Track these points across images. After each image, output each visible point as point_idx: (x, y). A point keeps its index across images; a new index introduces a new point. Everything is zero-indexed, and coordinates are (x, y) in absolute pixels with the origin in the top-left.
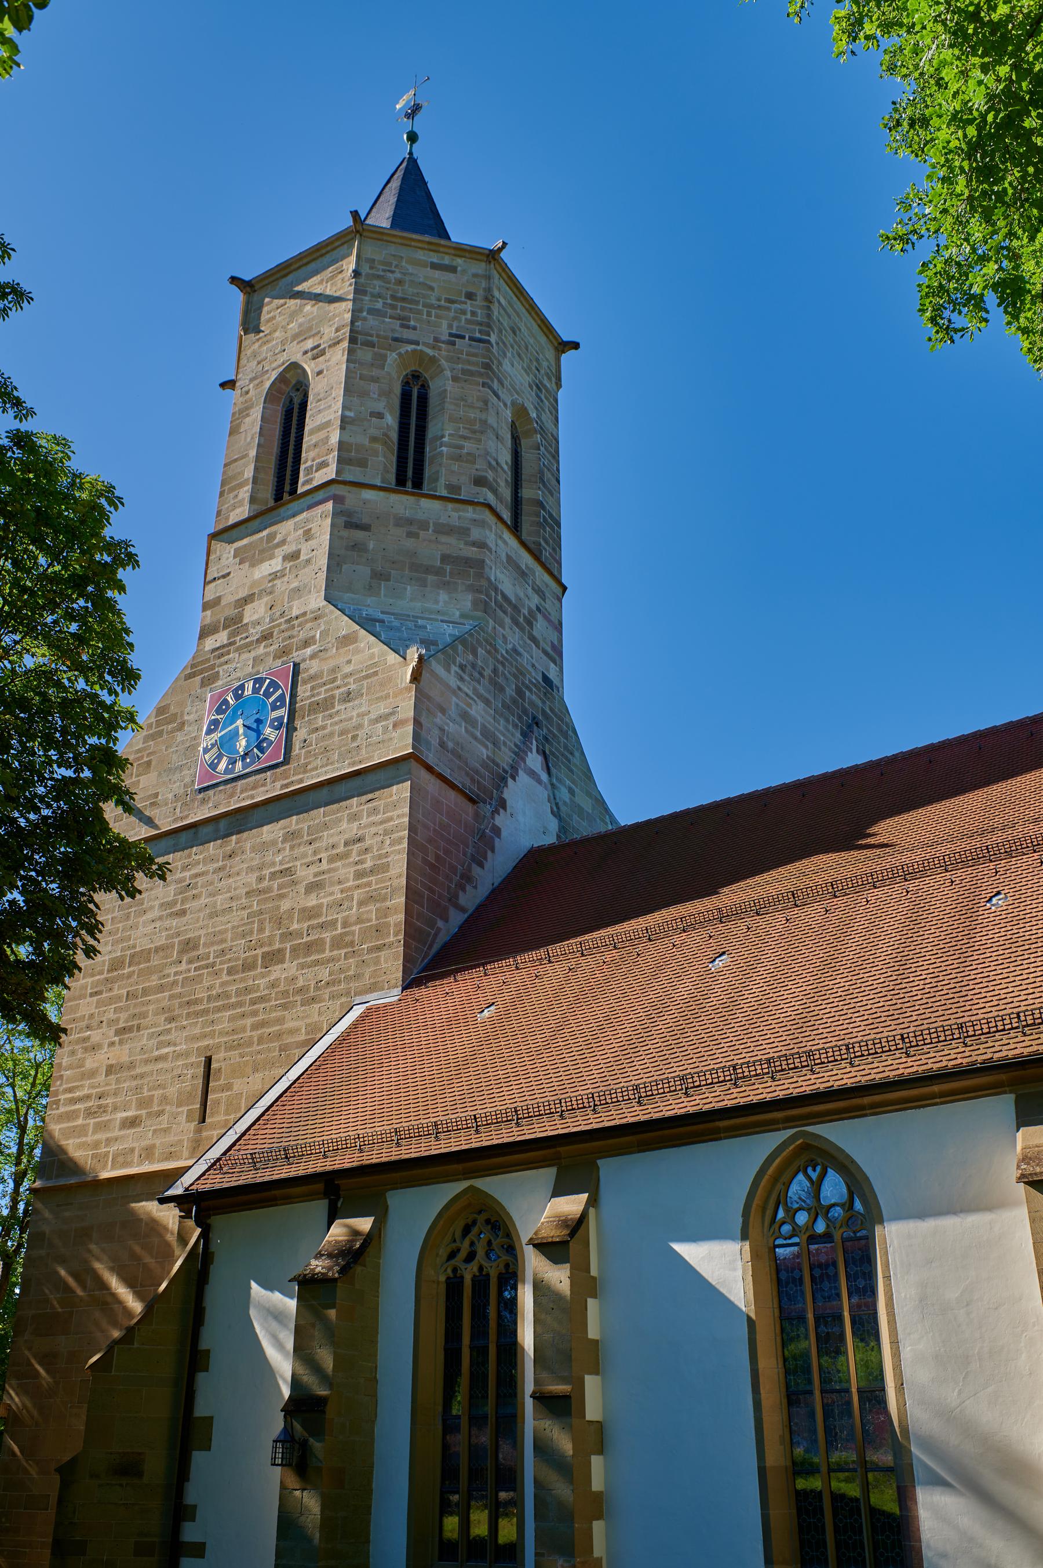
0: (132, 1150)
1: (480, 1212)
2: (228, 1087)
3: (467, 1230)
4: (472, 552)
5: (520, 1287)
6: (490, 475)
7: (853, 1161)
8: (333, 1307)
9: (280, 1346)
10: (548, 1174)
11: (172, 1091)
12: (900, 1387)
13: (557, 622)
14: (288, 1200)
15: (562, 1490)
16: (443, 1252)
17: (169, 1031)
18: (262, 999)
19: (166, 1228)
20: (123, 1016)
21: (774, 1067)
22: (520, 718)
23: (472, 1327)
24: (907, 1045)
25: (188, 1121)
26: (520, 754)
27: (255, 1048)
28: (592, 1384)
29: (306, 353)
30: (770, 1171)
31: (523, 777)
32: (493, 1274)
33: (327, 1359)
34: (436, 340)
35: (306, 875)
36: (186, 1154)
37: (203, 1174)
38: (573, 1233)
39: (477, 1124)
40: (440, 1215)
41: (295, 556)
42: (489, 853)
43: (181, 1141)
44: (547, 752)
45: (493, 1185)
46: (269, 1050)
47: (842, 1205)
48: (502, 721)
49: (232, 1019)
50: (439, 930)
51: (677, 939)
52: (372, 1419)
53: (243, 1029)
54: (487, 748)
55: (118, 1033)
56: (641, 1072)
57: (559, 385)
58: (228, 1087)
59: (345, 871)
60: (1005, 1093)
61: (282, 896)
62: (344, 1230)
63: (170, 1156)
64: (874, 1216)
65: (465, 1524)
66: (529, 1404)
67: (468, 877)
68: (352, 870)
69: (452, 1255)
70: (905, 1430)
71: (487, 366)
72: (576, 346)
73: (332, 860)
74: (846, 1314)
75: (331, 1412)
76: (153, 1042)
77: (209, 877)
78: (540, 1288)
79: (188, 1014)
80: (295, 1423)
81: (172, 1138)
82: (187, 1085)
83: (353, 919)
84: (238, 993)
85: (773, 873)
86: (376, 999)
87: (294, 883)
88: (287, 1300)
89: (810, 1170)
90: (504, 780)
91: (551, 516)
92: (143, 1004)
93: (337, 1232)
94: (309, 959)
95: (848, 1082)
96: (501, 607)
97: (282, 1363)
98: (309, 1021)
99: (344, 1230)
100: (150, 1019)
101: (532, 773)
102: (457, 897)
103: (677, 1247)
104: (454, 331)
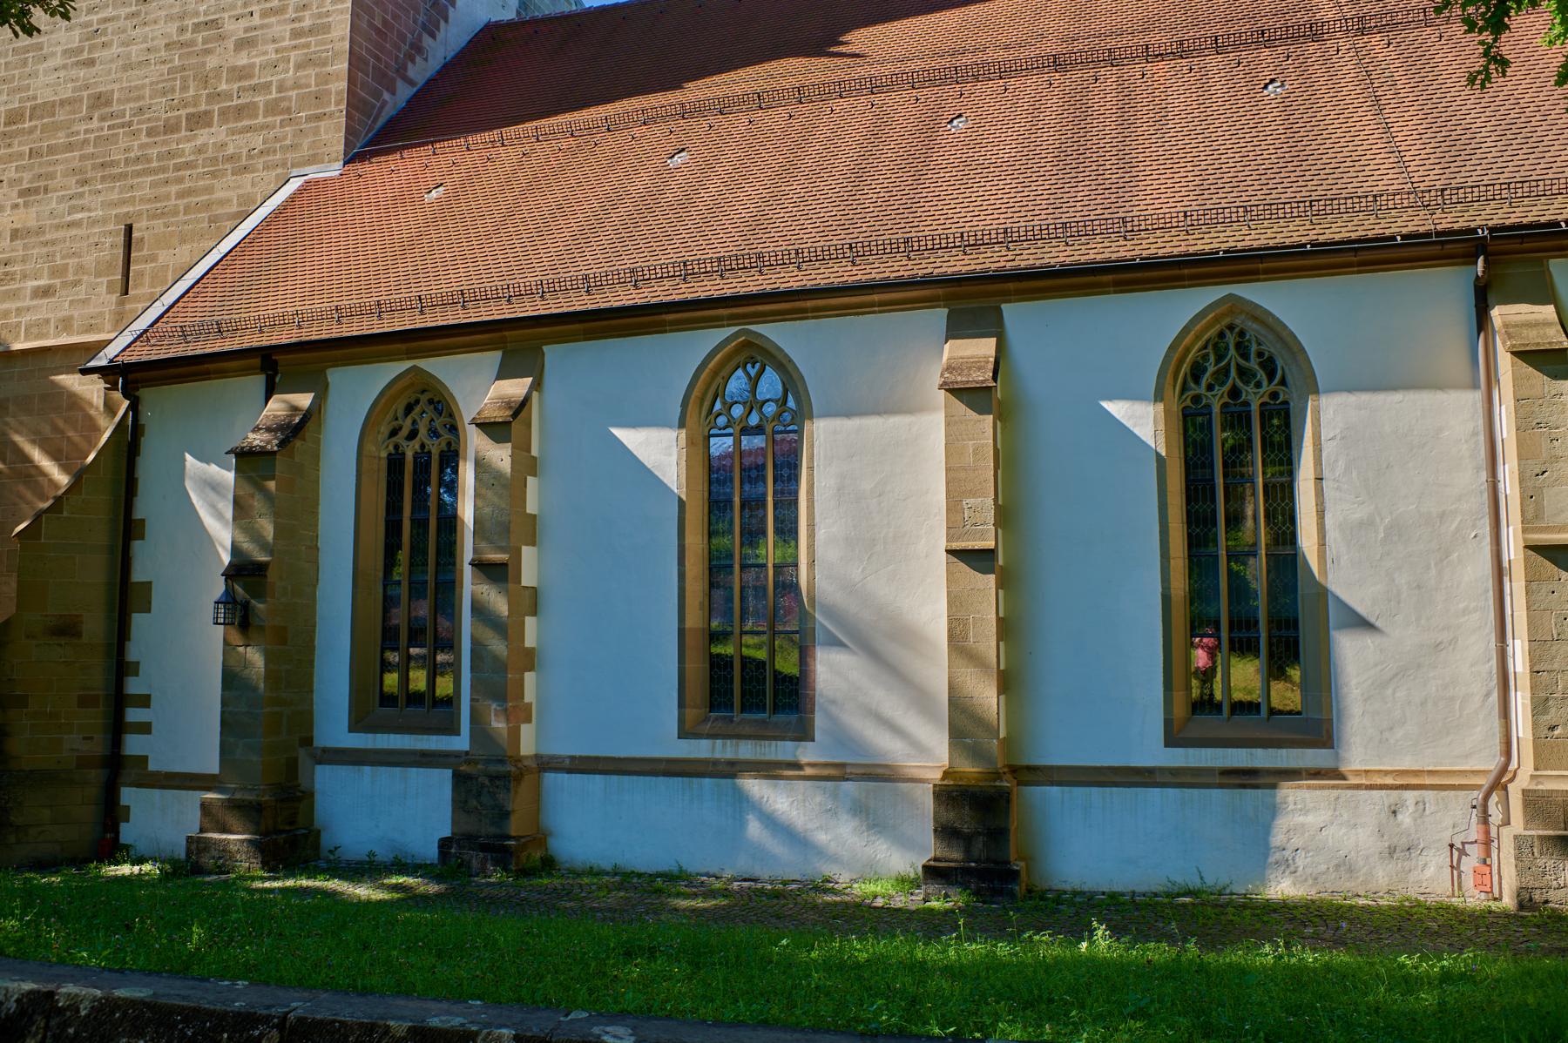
0: (47, 321)
1: (423, 392)
2: (153, 258)
3: (409, 409)
5: (461, 464)
7: (790, 361)
8: (273, 478)
9: (219, 516)
10: (494, 358)
11: (89, 260)
12: (812, 563)
14: (223, 374)
15: (498, 646)
16: (385, 430)
17: (81, 195)
18: (188, 165)
19: (91, 404)
20: (27, 176)
21: (724, 267)
23: (413, 501)
24: (854, 252)
25: (109, 292)
27: (181, 217)
28: (528, 553)
30: (711, 365)
32: (435, 452)
33: (268, 529)
35: (235, 29)
36: (108, 326)
37: (129, 346)
38: (515, 415)
39: (422, 305)
40: (382, 393)
42: (442, 23)
43: (101, 314)
45: (435, 366)
46: (198, 221)
47: (776, 401)
49: (153, 185)
50: (385, 103)
51: (636, 132)
52: (314, 583)
53: (168, 197)
55: (21, 194)
56: (591, 263)
58: (153, 258)
59: (280, 28)
61: (208, 52)
62: (283, 406)
63: (90, 328)
64: (804, 412)
65: (405, 680)
66: (467, 571)
67: (417, 48)
68: (289, 27)
69: (394, 433)
70: (812, 600)
73: (264, 14)
74: (770, 499)
75: (272, 575)
76: (64, 206)
77: (121, 23)
78: (480, 465)
79: (103, 177)
80: (237, 587)
81: (91, 310)
82: (105, 254)
83: (290, 83)
84: (160, 157)
85: (741, 72)
86: (315, 173)
87: (221, 37)
88: (224, 472)
89: (749, 367)
92: (49, 163)
93: (276, 407)
94: (240, 124)
95: (795, 285)
97: (222, 534)
98: (241, 192)
99: (283, 406)
100: (59, 181)
102: (405, 69)
103: (618, 432)
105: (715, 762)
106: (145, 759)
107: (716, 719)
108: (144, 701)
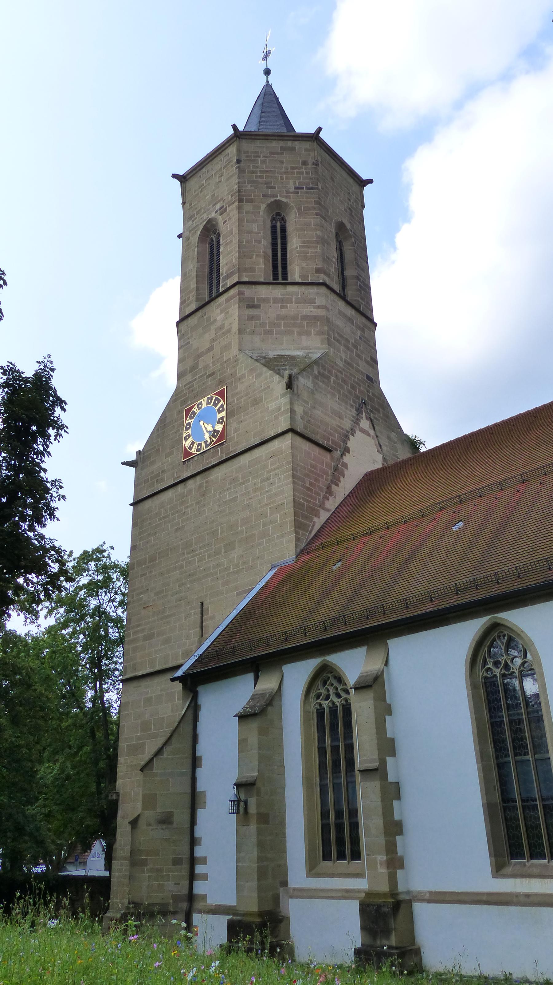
22: (354, 401)
26: (356, 421)
29: (217, 212)
31: (358, 434)
34: (287, 192)
41: (221, 327)
44: (372, 418)
48: (343, 404)
54: (335, 420)
60: (239, 888)
90: (347, 437)
96: (338, 341)
101: (363, 431)
102: (324, 503)
104: (297, 186)
105: (517, 895)
106: (204, 897)
107: (515, 864)
108: (204, 861)
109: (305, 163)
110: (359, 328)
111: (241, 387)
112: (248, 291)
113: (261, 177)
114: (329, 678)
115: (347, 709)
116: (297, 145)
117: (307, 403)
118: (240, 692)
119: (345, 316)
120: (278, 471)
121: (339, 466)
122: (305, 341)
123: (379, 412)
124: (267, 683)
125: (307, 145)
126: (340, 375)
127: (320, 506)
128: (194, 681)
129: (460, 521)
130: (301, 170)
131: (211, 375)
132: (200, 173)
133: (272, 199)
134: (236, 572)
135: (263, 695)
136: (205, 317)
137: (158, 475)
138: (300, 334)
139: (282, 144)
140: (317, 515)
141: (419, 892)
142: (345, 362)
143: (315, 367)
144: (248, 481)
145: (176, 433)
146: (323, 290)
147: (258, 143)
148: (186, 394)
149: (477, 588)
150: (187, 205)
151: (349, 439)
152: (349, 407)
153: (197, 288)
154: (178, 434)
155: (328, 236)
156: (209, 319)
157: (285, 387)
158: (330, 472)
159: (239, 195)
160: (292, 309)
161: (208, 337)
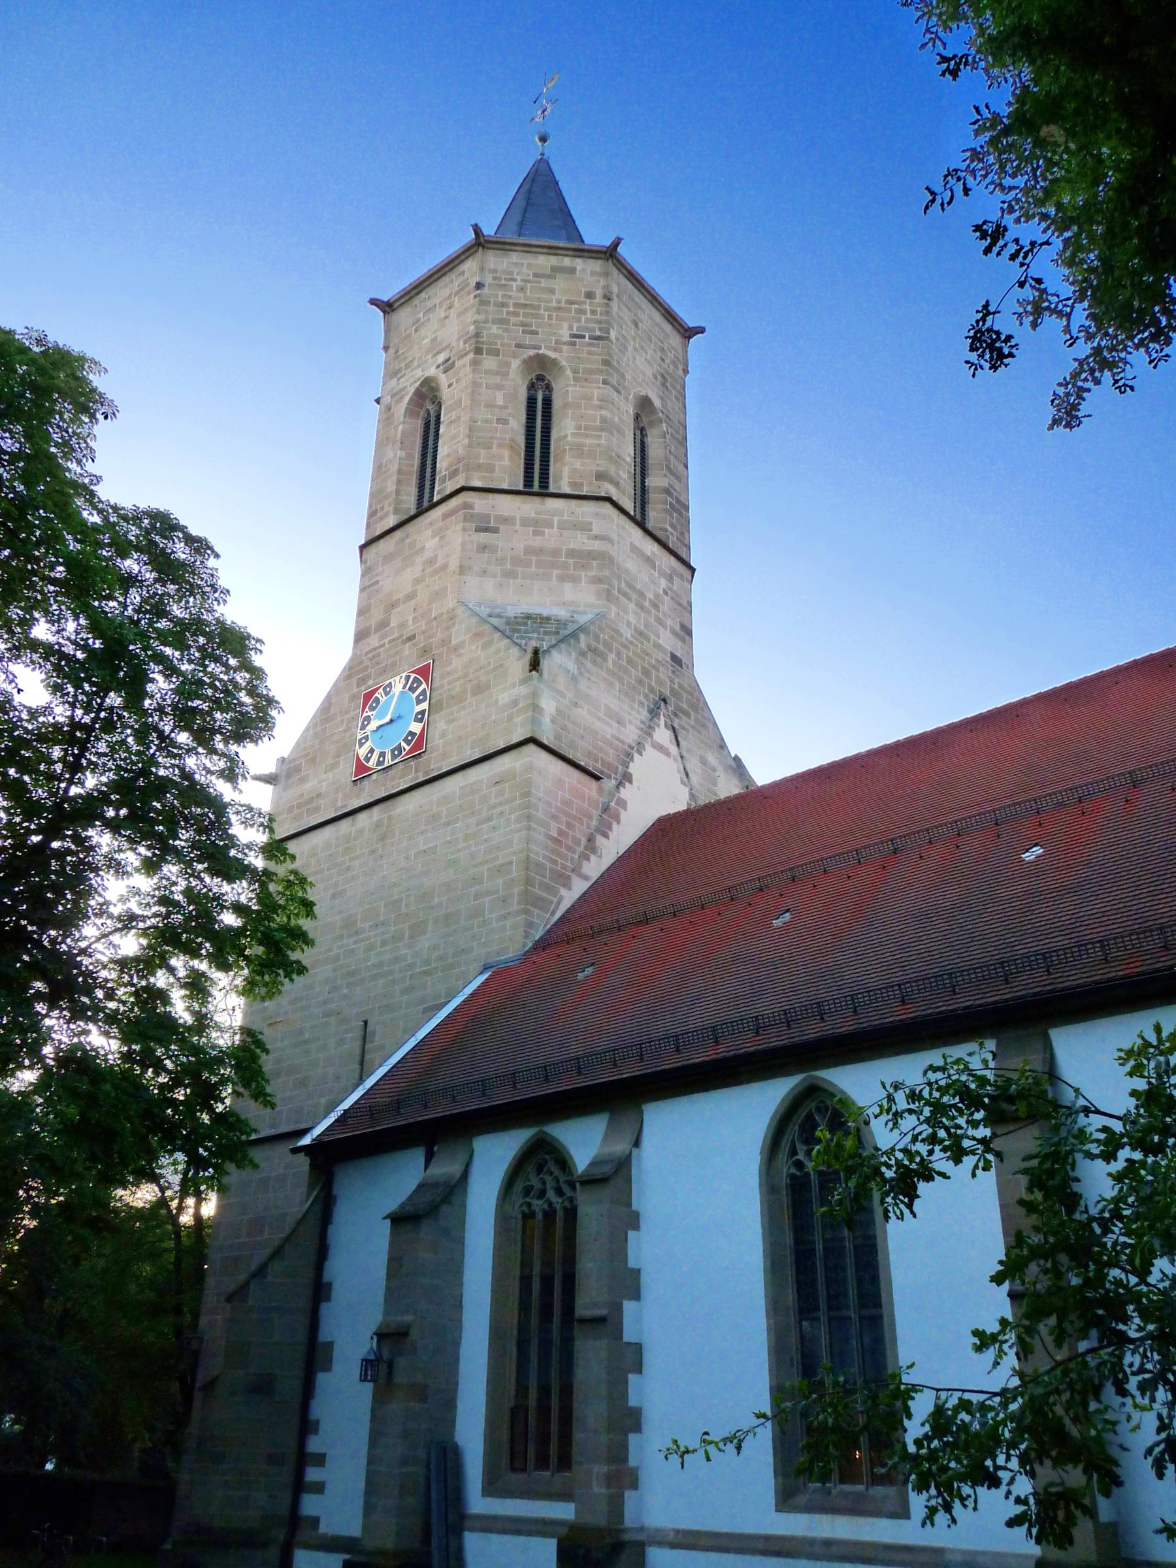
4: (596, 545)
6: (612, 470)
13: (685, 604)
22: (646, 696)
26: (648, 730)
29: (438, 366)
31: (649, 751)
41: (431, 562)
44: (676, 726)
54: (611, 727)
57: (686, 372)
60: (369, 1510)
71: (607, 363)
72: (701, 330)
90: (629, 756)
91: (678, 501)
96: (625, 595)
102: (580, 866)
105: (812, 1542)
106: (316, 1520)
109: (590, 295)
110: (662, 573)
111: (457, 663)
112: (480, 503)
113: (516, 314)
114: (546, 1161)
115: (571, 1214)
116: (579, 264)
117: (563, 695)
118: (402, 1177)
119: (641, 554)
120: (506, 808)
121: (613, 804)
122: (569, 592)
123: (689, 716)
124: (446, 1168)
125: (596, 265)
126: (624, 651)
127: (573, 870)
128: (331, 1158)
129: (788, 911)
130: (583, 307)
131: (410, 639)
132: (416, 301)
133: (532, 352)
134: (425, 973)
135: (436, 1184)
136: (407, 541)
137: (311, 800)
138: (562, 579)
139: (554, 260)
140: (567, 885)
141: (658, 1530)
142: (636, 629)
143: (582, 637)
144: (457, 820)
145: (345, 731)
146: (607, 508)
147: (515, 257)
148: (366, 668)
149: (789, 1026)
150: (392, 351)
151: (632, 759)
152: (636, 706)
153: (398, 492)
154: (348, 734)
155: (620, 418)
156: (412, 545)
157: (527, 667)
158: (595, 813)
159: (477, 342)
160: (550, 538)
161: (410, 575)
